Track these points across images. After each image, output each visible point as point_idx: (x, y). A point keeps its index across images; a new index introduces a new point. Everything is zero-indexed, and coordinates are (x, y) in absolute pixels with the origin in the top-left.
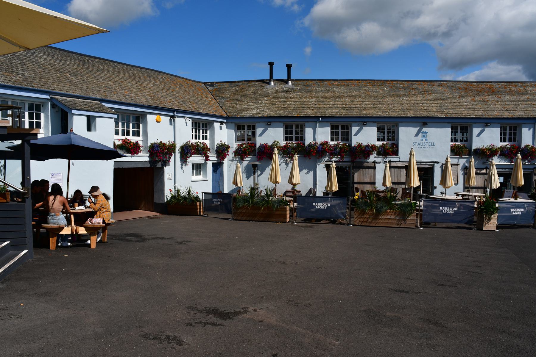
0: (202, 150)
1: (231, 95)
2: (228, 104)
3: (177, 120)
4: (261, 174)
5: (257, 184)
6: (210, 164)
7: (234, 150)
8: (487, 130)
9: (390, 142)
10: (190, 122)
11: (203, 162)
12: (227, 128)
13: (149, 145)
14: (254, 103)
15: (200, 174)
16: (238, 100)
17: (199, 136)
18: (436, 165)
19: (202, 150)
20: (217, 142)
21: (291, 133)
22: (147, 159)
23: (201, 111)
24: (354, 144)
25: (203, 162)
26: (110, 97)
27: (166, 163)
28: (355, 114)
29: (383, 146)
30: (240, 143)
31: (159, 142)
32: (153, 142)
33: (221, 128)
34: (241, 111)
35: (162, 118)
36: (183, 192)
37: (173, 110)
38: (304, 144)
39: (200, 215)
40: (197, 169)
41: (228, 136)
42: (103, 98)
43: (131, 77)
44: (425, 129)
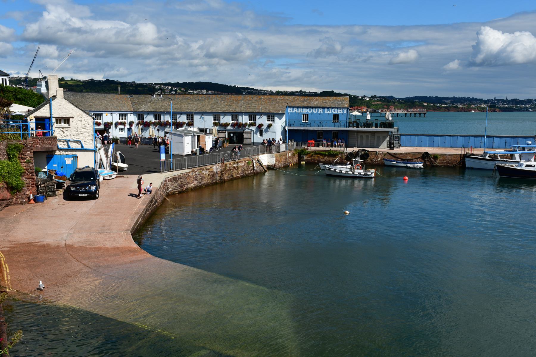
0: (123, 124)
1: (138, 101)
2: (135, 105)
3: (113, 114)
4: (146, 132)
5: (143, 136)
6: (126, 129)
7: (137, 123)
8: (226, 117)
9: (191, 121)
10: (118, 115)
11: (124, 128)
12: (134, 115)
13: (104, 123)
14: (145, 105)
15: (123, 132)
16: (140, 104)
17: (122, 119)
18: (207, 129)
19: (123, 124)
20: (129, 120)
21: (157, 117)
22: (103, 127)
23: (122, 110)
24: (178, 122)
25: (124, 128)
26: (92, 109)
27: (110, 128)
28: (178, 111)
29: (189, 122)
30: (139, 121)
31: (107, 122)
32: (105, 122)
33: (131, 115)
34: (139, 109)
35: (108, 114)
36: (115, 137)
37: (112, 111)
38: (161, 121)
39: (119, 144)
40: (121, 130)
41: (134, 118)
42: (90, 110)
43: (98, 99)
44: (203, 116)
